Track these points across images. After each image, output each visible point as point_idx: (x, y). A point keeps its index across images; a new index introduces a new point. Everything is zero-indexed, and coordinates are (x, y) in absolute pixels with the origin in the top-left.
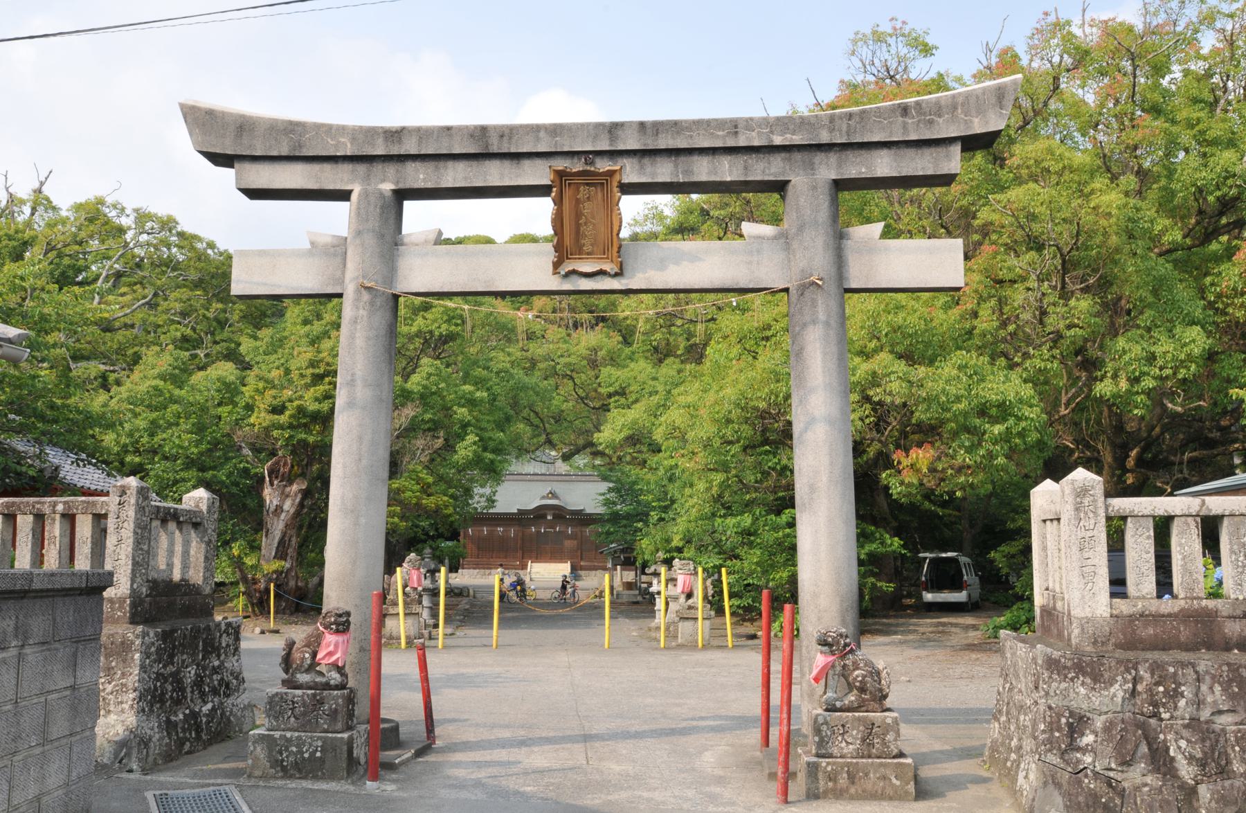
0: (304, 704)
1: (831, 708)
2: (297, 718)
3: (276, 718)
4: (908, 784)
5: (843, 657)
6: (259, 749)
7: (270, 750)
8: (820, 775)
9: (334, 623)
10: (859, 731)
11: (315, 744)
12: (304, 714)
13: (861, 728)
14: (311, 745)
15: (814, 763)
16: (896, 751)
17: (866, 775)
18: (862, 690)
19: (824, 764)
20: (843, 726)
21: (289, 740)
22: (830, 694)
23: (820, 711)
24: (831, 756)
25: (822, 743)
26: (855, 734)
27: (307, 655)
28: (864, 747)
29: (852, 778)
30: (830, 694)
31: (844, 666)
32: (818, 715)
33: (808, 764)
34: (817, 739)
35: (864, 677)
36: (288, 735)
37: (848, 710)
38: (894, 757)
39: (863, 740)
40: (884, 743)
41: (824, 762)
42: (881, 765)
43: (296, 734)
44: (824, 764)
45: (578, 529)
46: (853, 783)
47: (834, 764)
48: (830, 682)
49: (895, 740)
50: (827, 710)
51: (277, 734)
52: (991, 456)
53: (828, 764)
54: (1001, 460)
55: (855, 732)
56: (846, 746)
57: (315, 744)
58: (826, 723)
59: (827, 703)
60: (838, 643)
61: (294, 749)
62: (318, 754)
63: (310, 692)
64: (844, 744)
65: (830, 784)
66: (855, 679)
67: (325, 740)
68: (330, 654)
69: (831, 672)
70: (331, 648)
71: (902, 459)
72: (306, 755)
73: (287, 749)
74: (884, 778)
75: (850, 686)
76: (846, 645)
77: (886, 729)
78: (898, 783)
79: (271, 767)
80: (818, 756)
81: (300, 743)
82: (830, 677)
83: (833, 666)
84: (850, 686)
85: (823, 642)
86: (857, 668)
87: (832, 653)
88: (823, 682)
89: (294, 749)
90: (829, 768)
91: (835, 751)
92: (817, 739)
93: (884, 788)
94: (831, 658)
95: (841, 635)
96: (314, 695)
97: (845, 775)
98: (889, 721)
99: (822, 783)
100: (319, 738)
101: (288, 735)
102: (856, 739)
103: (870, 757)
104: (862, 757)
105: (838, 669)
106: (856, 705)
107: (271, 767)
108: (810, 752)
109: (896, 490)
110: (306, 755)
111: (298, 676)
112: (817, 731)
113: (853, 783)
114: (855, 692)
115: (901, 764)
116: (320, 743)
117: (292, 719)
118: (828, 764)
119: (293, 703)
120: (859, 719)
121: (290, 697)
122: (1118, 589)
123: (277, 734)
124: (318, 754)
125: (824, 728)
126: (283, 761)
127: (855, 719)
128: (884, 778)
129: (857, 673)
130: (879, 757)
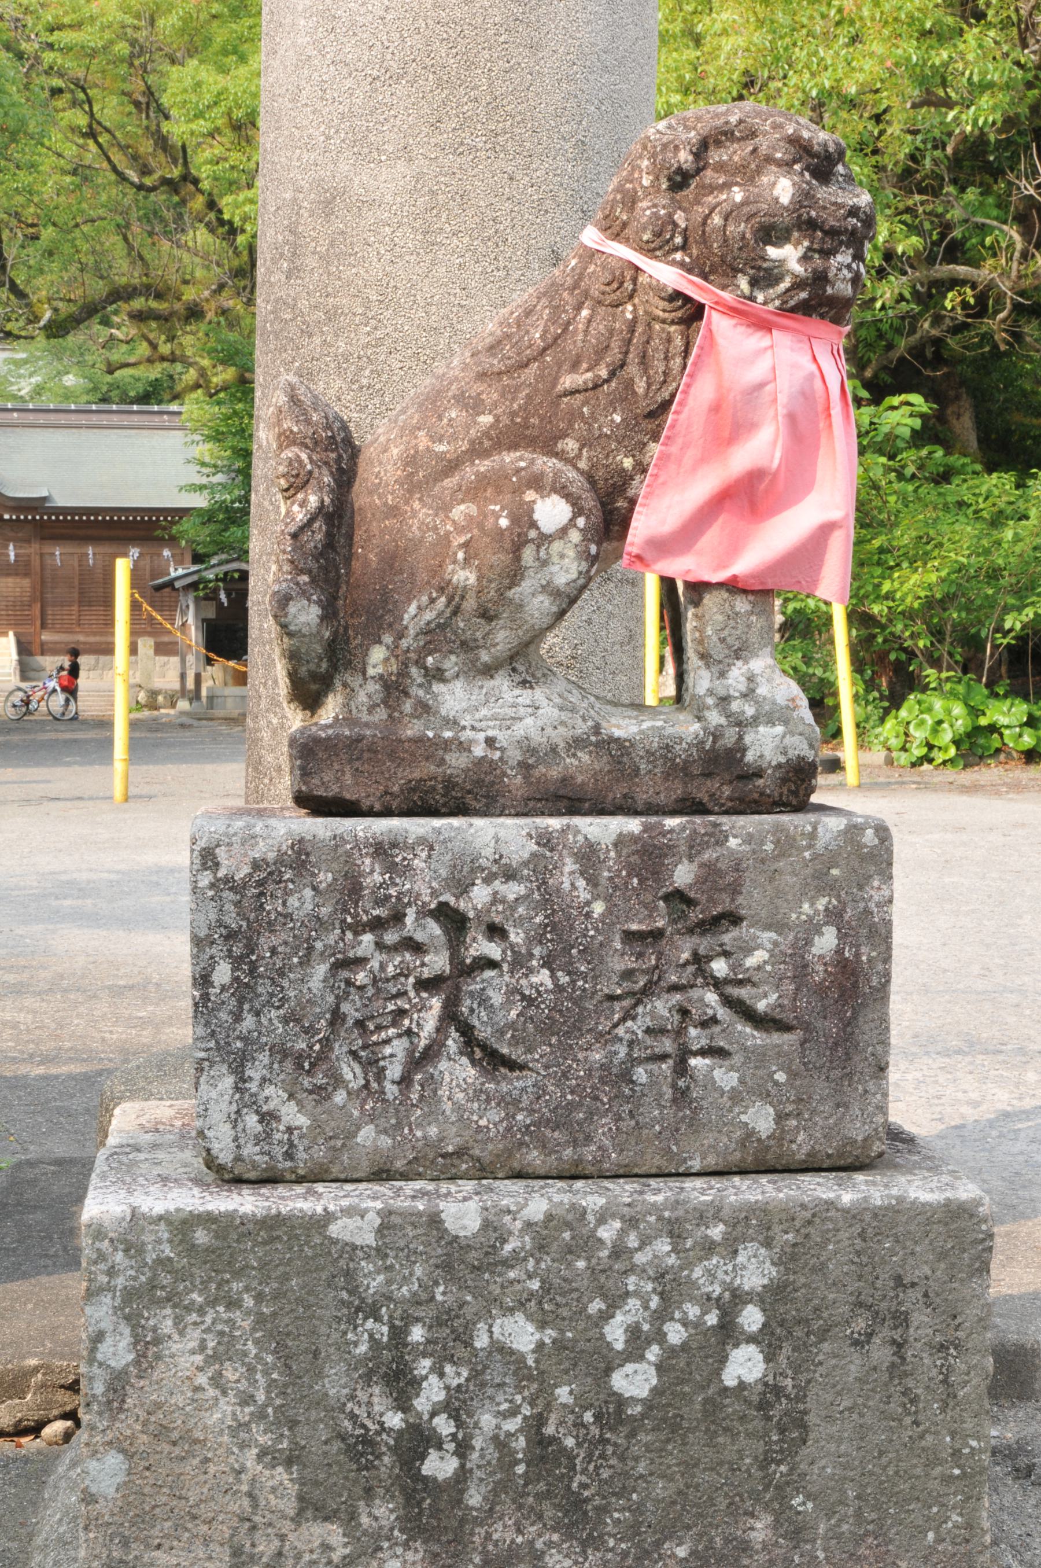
0: (560, 936)
2: (493, 1061)
3: (309, 1068)
6: (184, 1353)
7: (295, 1359)
9: (804, 222)
11: (708, 1276)
12: (562, 1022)
14: (671, 1288)
21: (467, 1262)
27: (551, 512)
36: (463, 1210)
43: (538, 1202)
45: (33, 549)
51: (352, 1212)
57: (708, 1276)
61: (522, 1335)
62: (745, 1365)
63: (603, 830)
67: (799, 1243)
68: (749, 497)
70: (761, 447)
72: (635, 1382)
73: (452, 1336)
79: (311, 1507)
81: (572, 1277)
89: (522, 1335)
96: (648, 858)
100: (751, 1225)
101: (463, 1210)
107: (311, 1507)
110: (635, 1382)
111: (454, 698)
116: (754, 1270)
117: (457, 1072)
119: (454, 922)
121: (424, 883)
122: (882, 834)
123: (352, 1212)
124: (745, 1365)
126: (418, 1441)
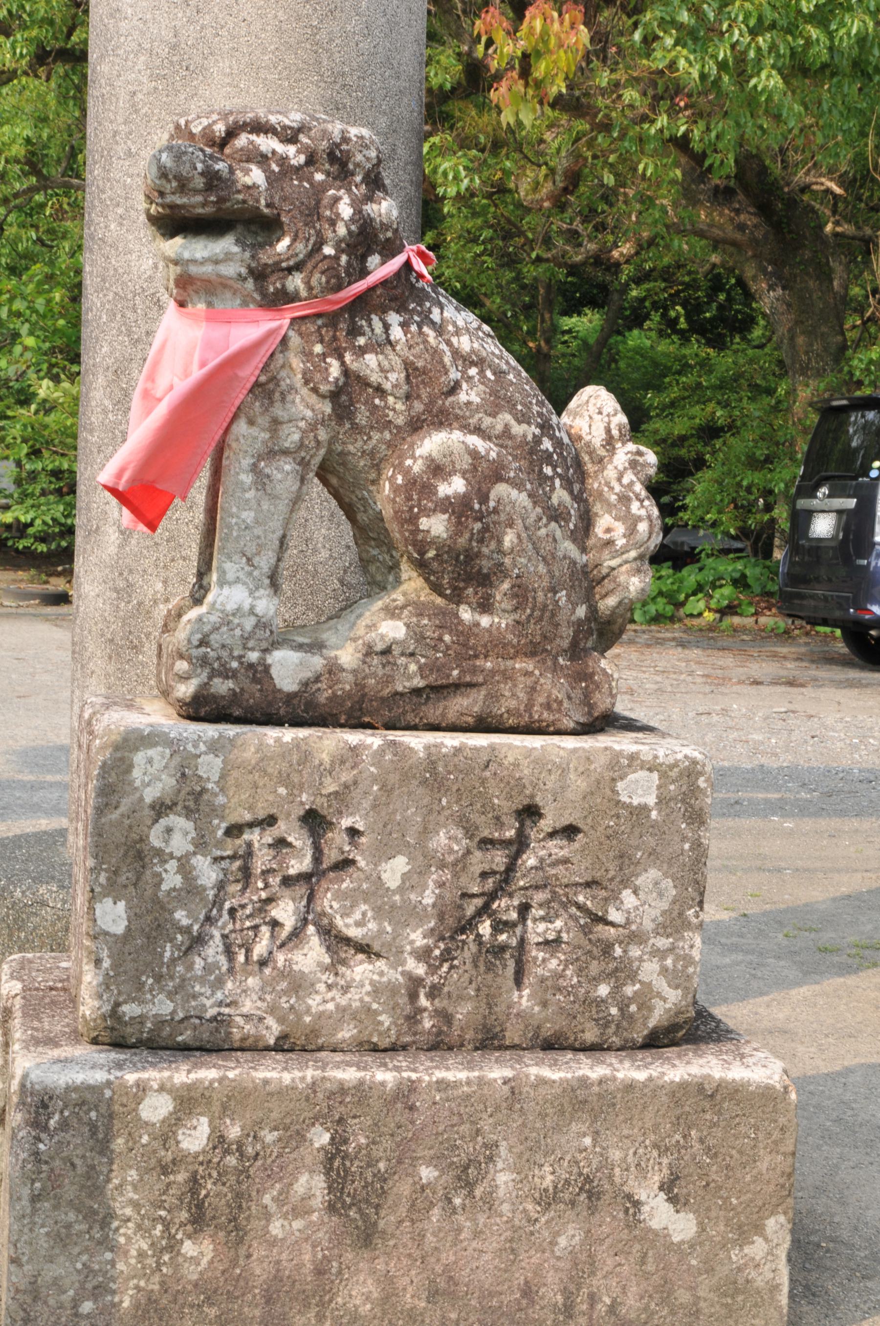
1: (232, 700)
4: (748, 1229)
5: (345, 321)
8: (127, 1190)
10: (425, 861)
13: (446, 840)
15: (85, 1098)
16: (667, 1002)
17: (467, 1176)
18: (463, 572)
19: (156, 1109)
20: (315, 821)
22: (234, 595)
23: (156, 716)
24: (213, 1041)
25: (149, 946)
26: (399, 881)
28: (459, 976)
29: (356, 1201)
30: (234, 595)
31: (347, 395)
32: (131, 742)
33: (40, 1104)
34: (114, 916)
35: (485, 475)
37: (355, 712)
38: (658, 1041)
39: (455, 927)
40: (599, 948)
41: (155, 1087)
42: (578, 1101)
44: (156, 1109)
46: (367, 1237)
47: (233, 1100)
48: (242, 510)
49: (674, 923)
50: (202, 709)
52: (741, 67)
53: (188, 1102)
54: (768, 80)
55: (394, 871)
56: (334, 971)
58: (191, 799)
59: (203, 653)
60: (314, 211)
64: (311, 954)
65: (198, 1252)
66: (420, 489)
69: (247, 436)
71: (500, 36)
74: (589, 1192)
75: (376, 552)
76: (367, 239)
77: (618, 842)
78: (680, 1226)
80: (118, 1037)
82: (240, 472)
83: (266, 389)
84: (376, 552)
85: (199, 205)
86: (442, 418)
87: (267, 288)
88: (185, 517)
90: (195, 1138)
91: (249, 1003)
92: (114, 916)
93: (582, 1266)
94: (251, 329)
95: (338, 160)
97: (311, 1184)
98: (640, 790)
99: (133, 1242)
102: (406, 915)
103: (490, 1041)
104: (439, 1045)
105: (304, 407)
106: (410, 675)
108: (65, 994)
109: (184, 1145)
112: (125, 858)
113: (367, 1237)
114: (412, 585)
115: (710, 1095)
118: (188, 1102)
120: (433, 774)
125: (177, 835)
127: (405, 772)
128: (589, 1192)
129: (433, 443)
130: (552, 1045)
